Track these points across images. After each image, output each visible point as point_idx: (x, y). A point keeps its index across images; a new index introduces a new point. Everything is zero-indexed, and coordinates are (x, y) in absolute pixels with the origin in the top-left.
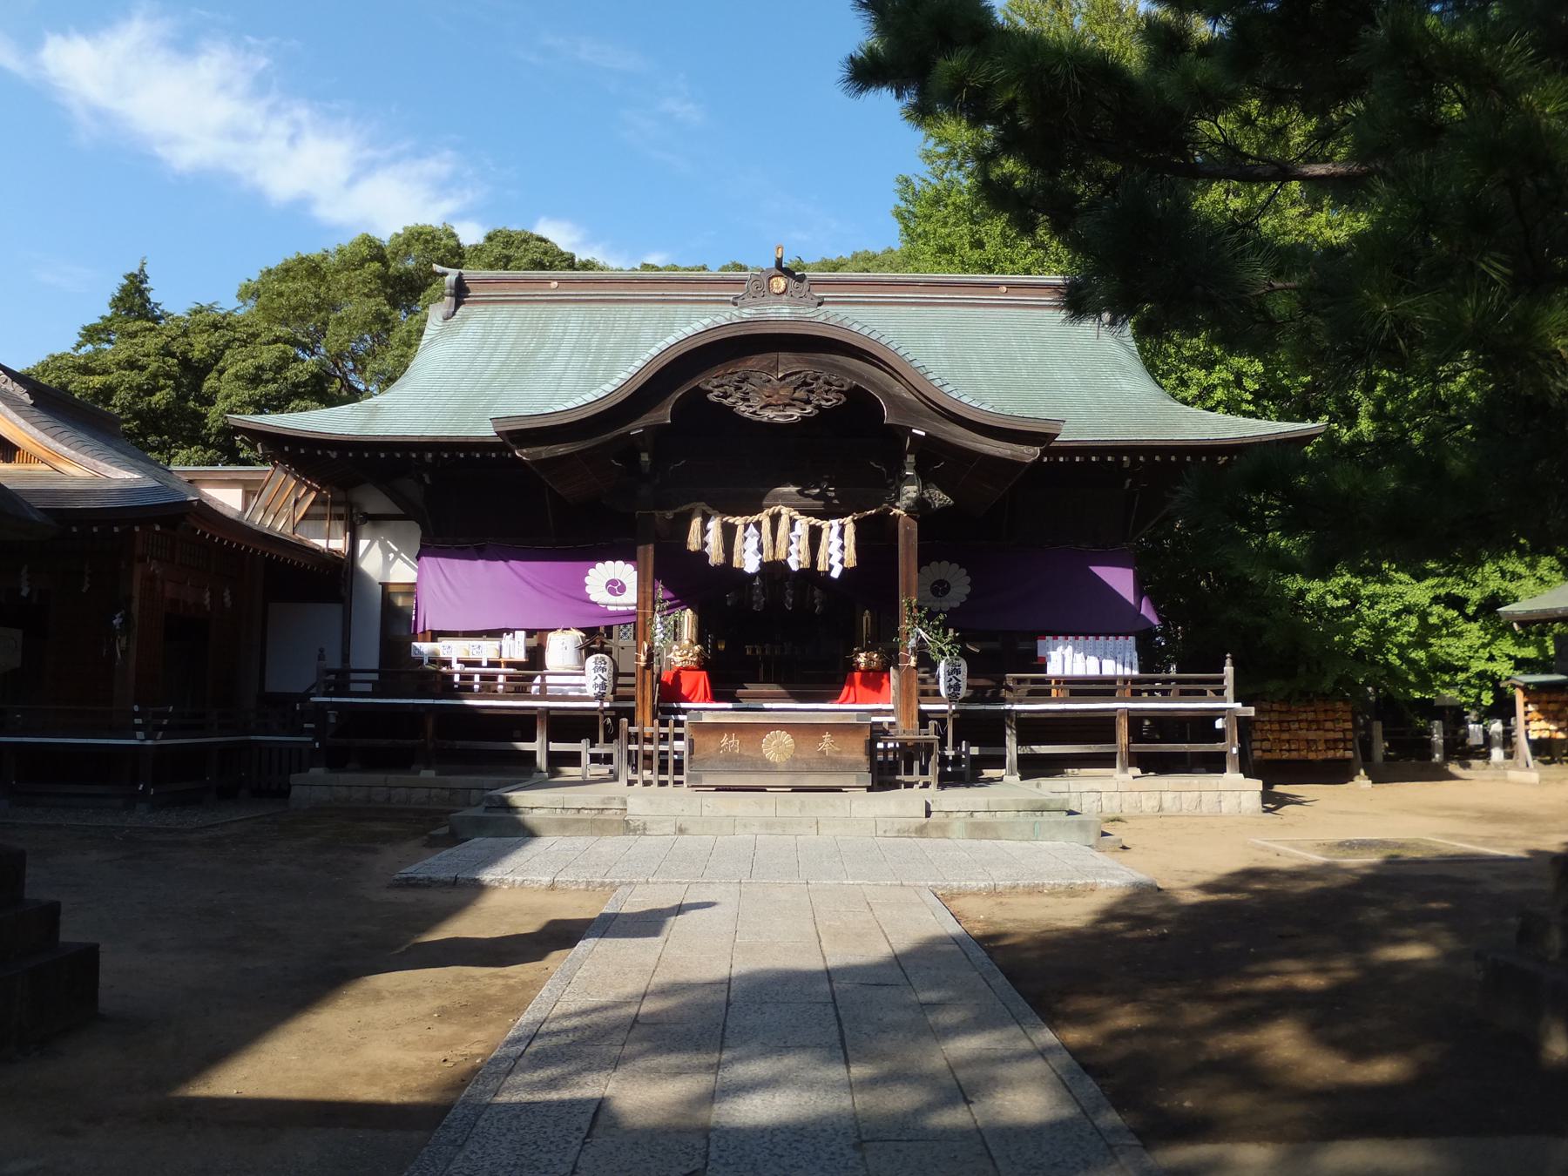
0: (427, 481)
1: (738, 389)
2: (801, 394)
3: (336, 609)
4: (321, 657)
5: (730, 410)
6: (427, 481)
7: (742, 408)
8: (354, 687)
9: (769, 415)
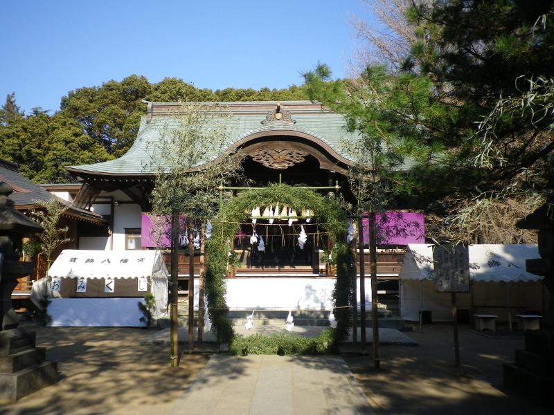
1: (264, 156)
2: (288, 157)
5: (261, 164)
7: (266, 164)
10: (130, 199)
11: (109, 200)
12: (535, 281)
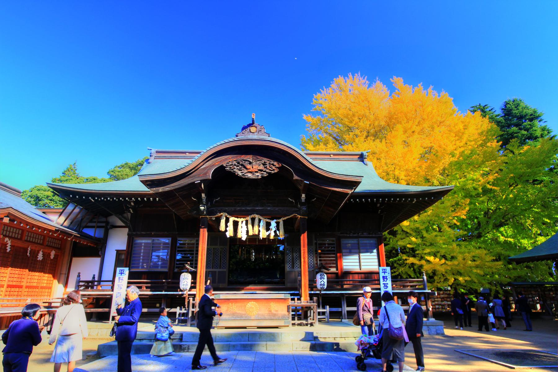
0: (131, 211)
3: (98, 260)
4: (79, 276)
5: (442, 312)
6: (131, 211)
7: (240, 173)
8: (345, 286)
9: (250, 175)
10: (122, 224)
11: (104, 224)
12: (75, 260)
